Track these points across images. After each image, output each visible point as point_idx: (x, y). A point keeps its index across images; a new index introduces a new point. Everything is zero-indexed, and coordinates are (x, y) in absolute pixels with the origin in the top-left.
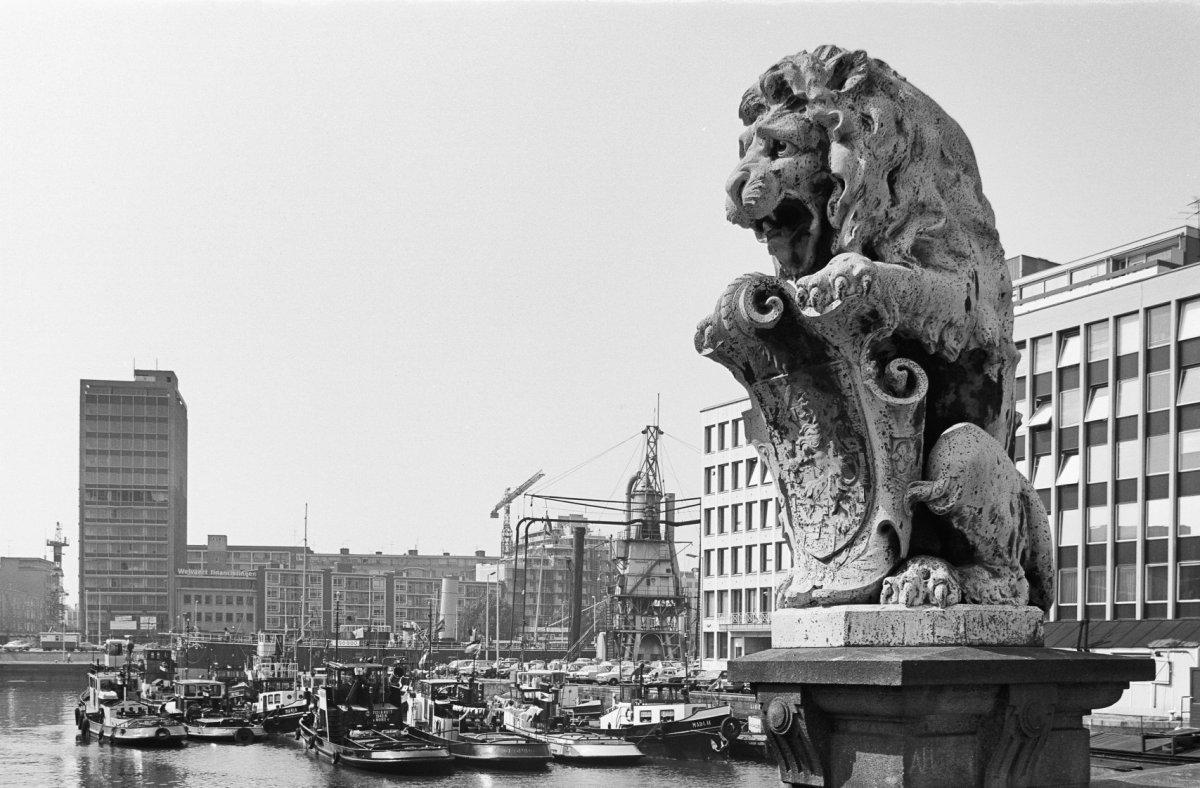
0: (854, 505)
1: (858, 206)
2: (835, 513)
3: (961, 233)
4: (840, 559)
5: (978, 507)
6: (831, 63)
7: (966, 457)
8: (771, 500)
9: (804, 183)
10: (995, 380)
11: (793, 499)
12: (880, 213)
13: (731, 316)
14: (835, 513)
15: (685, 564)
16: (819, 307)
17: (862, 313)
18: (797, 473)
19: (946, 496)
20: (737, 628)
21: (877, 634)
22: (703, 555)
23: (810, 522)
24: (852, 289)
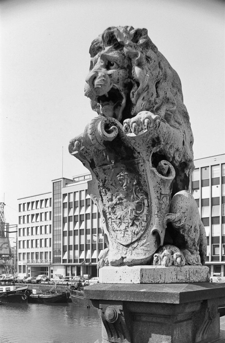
0: (141, 223)
1: (145, 94)
2: (132, 226)
3: (178, 115)
4: (135, 245)
5: (191, 226)
6: (132, 32)
7: (188, 204)
8: (39, 226)
9: (121, 82)
10: (188, 176)
11: (110, 219)
12: (153, 99)
13: (93, 133)
14: (132, 226)
15: (12, 245)
16: (136, 132)
17: (154, 137)
18: (113, 208)
19: (180, 220)
20: (28, 264)
21: (154, 278)
22: (18, 242)
23: (119, 229)
24: (152, 125)
